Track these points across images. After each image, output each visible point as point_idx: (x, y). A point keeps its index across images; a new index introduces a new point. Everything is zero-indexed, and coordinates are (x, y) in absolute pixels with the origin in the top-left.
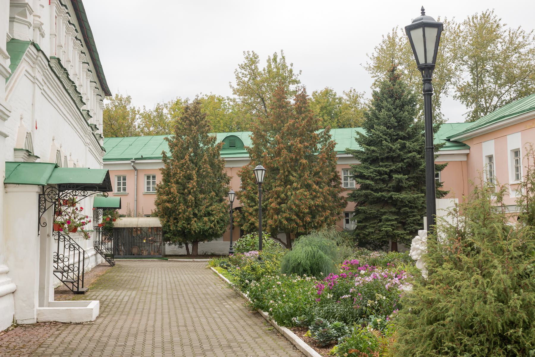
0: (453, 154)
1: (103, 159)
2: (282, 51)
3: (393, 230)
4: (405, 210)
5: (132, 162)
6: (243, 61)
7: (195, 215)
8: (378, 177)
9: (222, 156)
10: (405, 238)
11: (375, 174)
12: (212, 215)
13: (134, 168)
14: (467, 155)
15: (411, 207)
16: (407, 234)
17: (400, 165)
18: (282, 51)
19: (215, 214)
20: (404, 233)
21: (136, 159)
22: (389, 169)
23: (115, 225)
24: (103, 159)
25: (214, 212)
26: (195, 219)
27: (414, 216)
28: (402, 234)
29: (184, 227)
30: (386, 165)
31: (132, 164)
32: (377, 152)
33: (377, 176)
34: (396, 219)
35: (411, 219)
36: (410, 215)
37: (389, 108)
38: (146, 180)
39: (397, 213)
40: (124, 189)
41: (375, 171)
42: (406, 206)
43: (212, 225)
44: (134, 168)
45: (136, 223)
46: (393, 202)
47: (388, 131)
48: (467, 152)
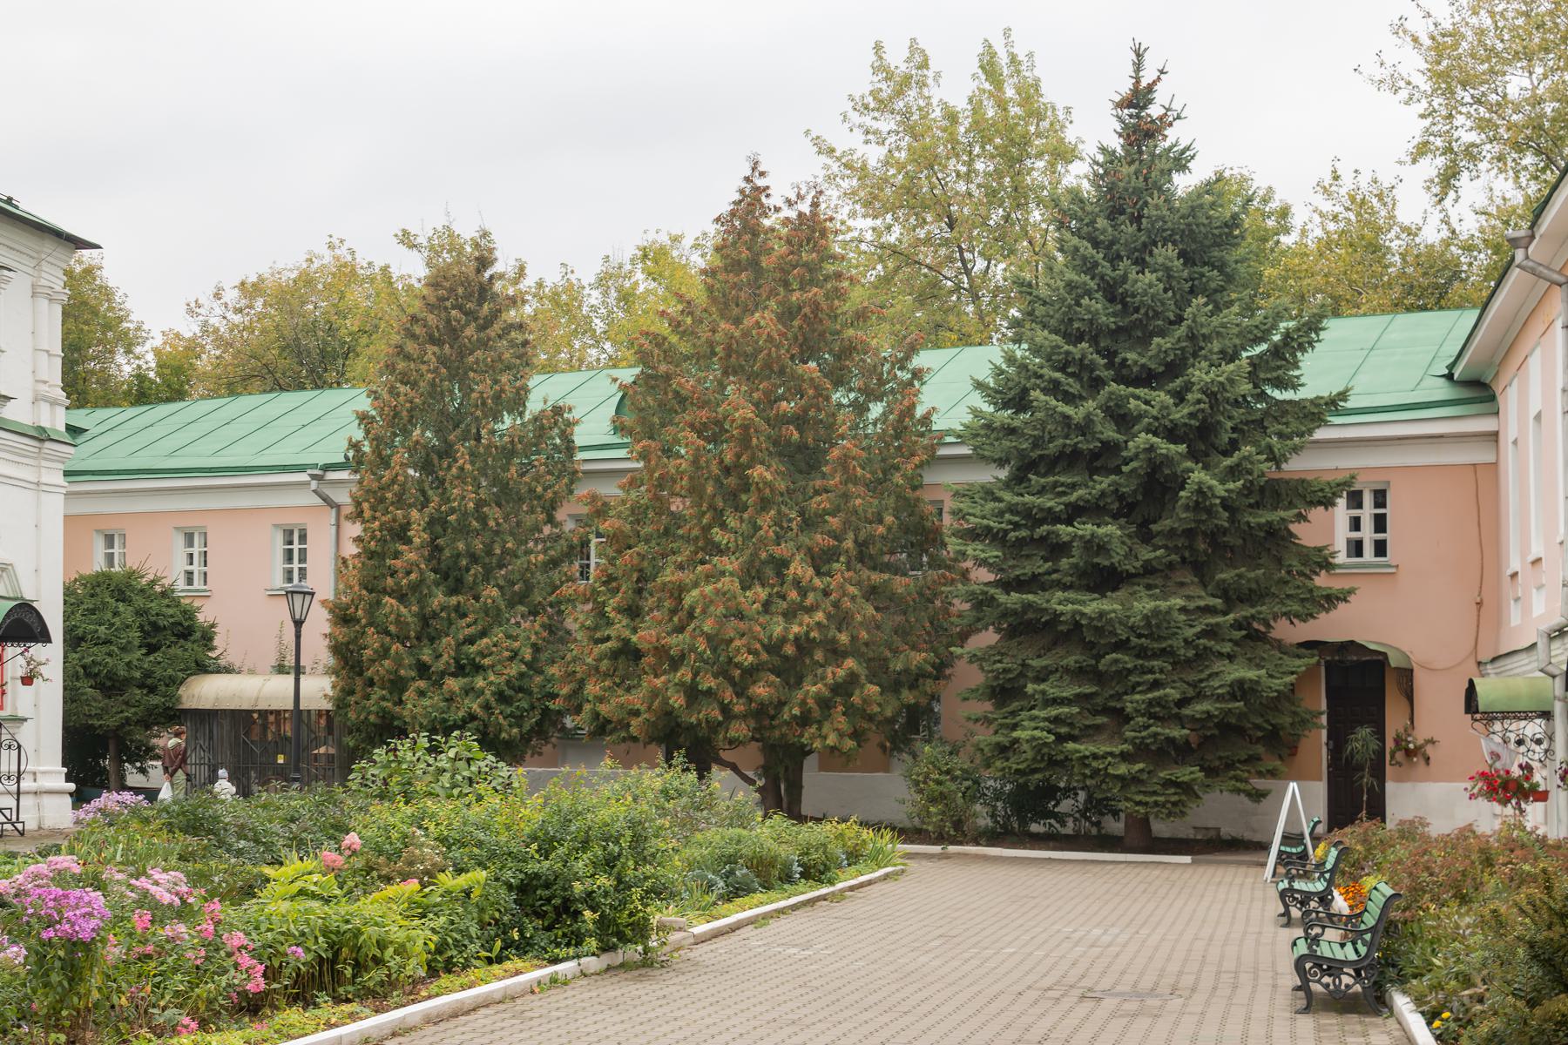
0: (1441, 436)
1: (67, 474)
2: (1007, 33)
3: (1061, 739)
4: (1116, 661)
5: (313, 477)
6: (864, 83)
7: (423, 669)
8: (1024, 533)
9: (580, 456)
10: (1111, 771)
11: (1010, 522)
12: (478, 669)
13: (325, 499)
14: (1494, 436)
15: (1142, 653)
16: (1124, 757)
17: (1103, 483)
18: (1007, 33)
19: (493, 666)
20: (1111, 754)
21: (328, 468)
22: (1064, 499)
23: (184, 699)
24: (67, 474)
25: (487, 662)
26: (422, 684)
27: (1156, 685)
28: (1095, 756)
29: (383, 709)
30: (1055, 484)
31: (314, 484)
32: (1023, 435)
33: (1017, 526)
34: (1079, 699)
35: (1137, 697)
36: (1139, 684)
37: (1084, 258)
38: (279, 546)
39: (1079, 673)
40: (1380, 548)
41: (1012, 509)
42: (1121, 646)
43: (475, 707)
44: (325, 499)
45: (255, 694)
46: (1073, 632)
47: (1068, 353)
48: (1485, 425)
